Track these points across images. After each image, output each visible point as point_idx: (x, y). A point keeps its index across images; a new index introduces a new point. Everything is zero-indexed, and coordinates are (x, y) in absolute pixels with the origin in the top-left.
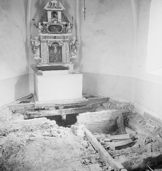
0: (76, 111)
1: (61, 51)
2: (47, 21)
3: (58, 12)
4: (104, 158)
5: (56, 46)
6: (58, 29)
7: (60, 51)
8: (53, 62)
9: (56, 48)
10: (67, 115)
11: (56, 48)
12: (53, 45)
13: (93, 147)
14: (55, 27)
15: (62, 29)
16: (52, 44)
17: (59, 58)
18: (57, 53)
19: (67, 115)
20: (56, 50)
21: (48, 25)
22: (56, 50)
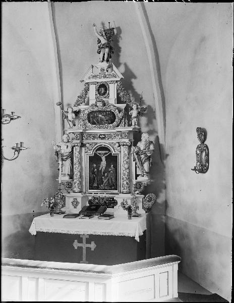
0: (78, 176)
1: (116, 167)
2: (88, 104)
3: (110, 85)
4: (103, 199)
5: (106, 154)
6: (108, 118)
7: (112, 166)
8: (97, 188)
9: (103, 158)
10: (78, 247)
11: (103, 158)
12: (100, 152)
13: (154, 287)
14: (100, 116)
15: (115, 117)
16: (96, 151)
17: (110, 181)
18: (106, 171)
19: (78, 247)
20: (104, 163)
21: (86, 112)
22: (104, 163)
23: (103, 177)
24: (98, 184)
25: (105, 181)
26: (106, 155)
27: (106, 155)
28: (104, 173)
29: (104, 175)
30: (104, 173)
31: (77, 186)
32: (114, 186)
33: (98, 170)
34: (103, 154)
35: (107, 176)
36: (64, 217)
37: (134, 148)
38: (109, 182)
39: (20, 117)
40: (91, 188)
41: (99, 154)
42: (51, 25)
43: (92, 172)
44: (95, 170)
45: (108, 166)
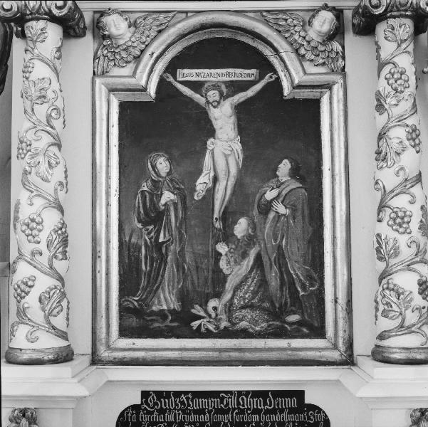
7: (285, 167)
8: (182, 324)
9: (223, 117)
11: (223, 117)
16: (172, 68)
20: (225, 149)
22: (225, 149)
23: (222, 248)
24: (184, 297)
25: (236, 271)
26: (241, 97)
27: (241, 97)
28: (229, 217)
29: (227, 236)
30: (229, 217)
31: (36, 313)
32: (294, 306)
33: (184, 194)
34: (215, 86)
35: (251, 240)
36: (79, 382)
37: (172, 307)
38: (263, 283)
39: (396, 152)
40: (133, 321)
41: (196, 86)
42: (319, 82)
43: (142, 210)
44: (167, 196)
45: (257, 161)
